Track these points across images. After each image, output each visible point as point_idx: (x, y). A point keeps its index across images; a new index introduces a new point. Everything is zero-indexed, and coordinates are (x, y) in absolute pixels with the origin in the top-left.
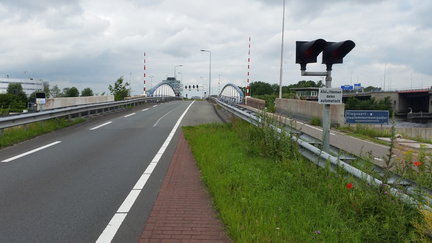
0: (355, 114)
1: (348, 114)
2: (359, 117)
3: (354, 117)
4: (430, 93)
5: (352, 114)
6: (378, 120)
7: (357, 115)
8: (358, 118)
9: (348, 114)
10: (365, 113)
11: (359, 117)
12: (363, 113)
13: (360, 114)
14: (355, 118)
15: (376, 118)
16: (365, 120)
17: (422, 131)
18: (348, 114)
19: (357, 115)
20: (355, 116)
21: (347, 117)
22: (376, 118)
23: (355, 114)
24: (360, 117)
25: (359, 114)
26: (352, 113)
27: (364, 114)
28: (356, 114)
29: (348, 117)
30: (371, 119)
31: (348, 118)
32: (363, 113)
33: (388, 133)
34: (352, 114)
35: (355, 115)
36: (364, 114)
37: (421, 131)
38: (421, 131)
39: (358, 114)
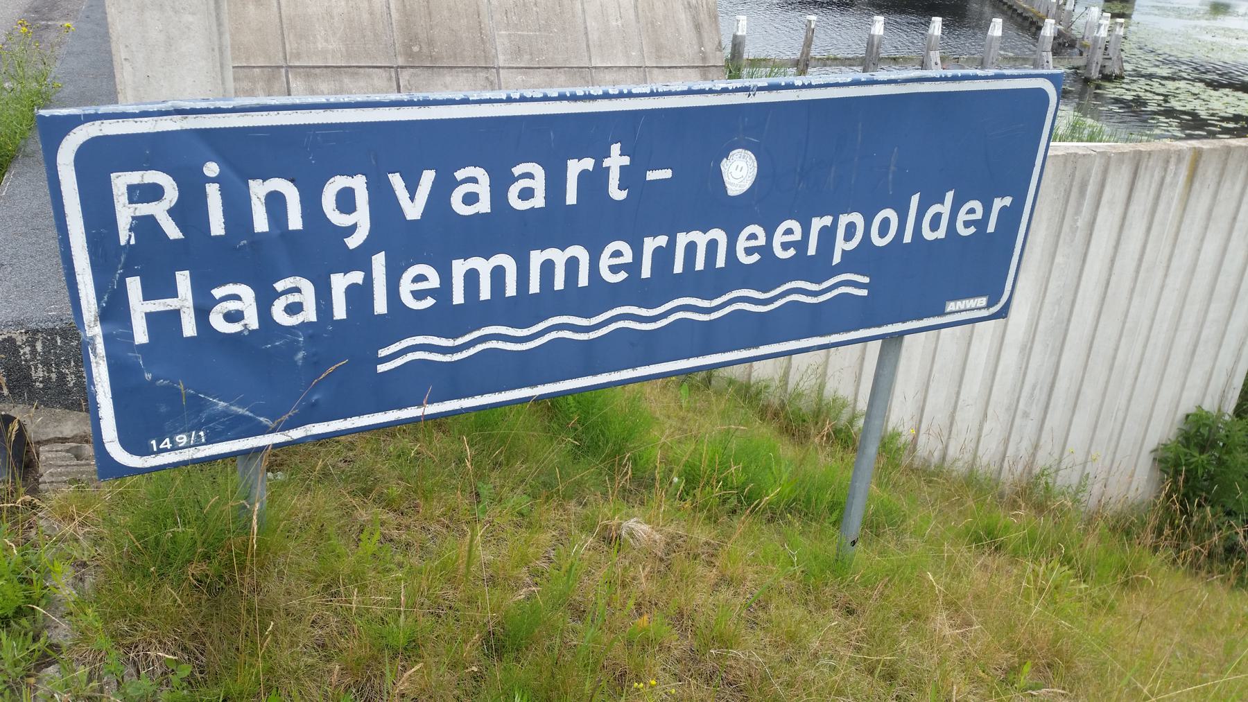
0: (346, 201)
1: (146, 226)
2: (459, 268)
3: (340, 283)
4: (382, 355)
5: (275, 202)
6: (851, 261)
7: (413, 210)
8: (444, 292)
9: (146, 226)
10: (616, 160)
11: (459, 268)
12: (575, 168)
13: (483, 188)
14: (360, 296)
15: (827, 235)
16: (615, 295)
17: (1109, 180)
18: (125, 214)
19: (413, 210)
20: (359, 261)
21: (139, 307)
22: (827, 235)
23: (346, 201)
24: (484, 267)
25: (531, 175)
26: (258, 190)
27: (593, 182)
28: (383, 202)
29: (159, 287)
30: (735, 275)
31: (164, 323)
32: (575, 168)
33: (851, 422)
34: (275, 202)
35: (362, 217)
36: (593, 182)
37: (1105, 171)
38: (1105, 171)
39: (443, 187)
